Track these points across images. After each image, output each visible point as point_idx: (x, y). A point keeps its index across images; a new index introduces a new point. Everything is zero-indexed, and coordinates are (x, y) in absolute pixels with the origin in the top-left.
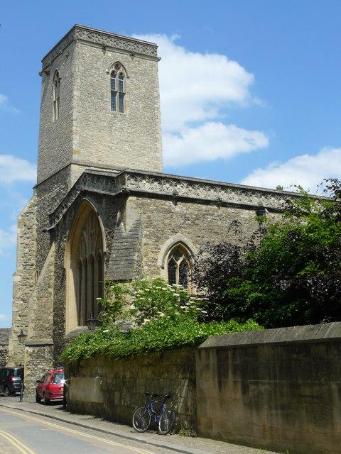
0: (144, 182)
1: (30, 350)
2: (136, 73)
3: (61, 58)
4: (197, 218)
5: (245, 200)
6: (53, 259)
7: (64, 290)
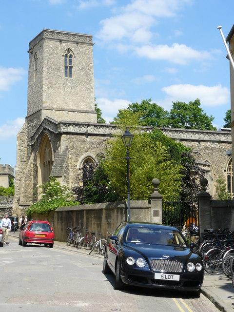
0: (70, 127)
1: (21, 208)
3: (38, 46)
6: (32, 161)
7: (37, 178)
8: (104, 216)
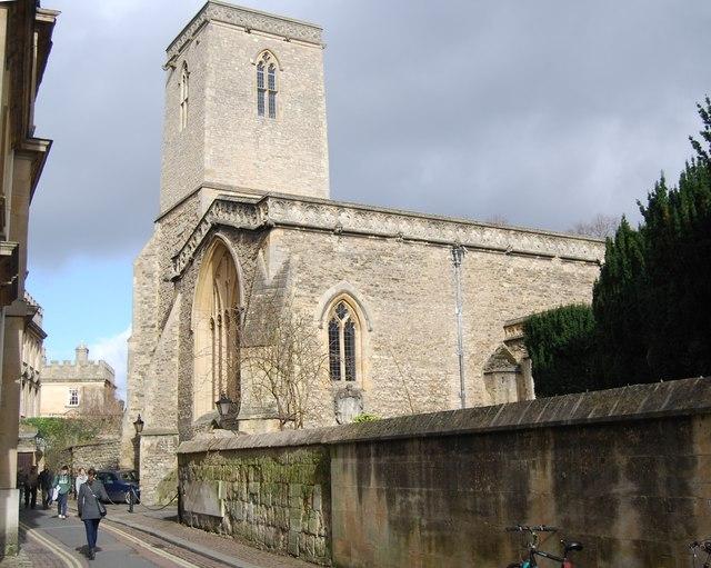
4: (369, 260)
5: (435, 234)
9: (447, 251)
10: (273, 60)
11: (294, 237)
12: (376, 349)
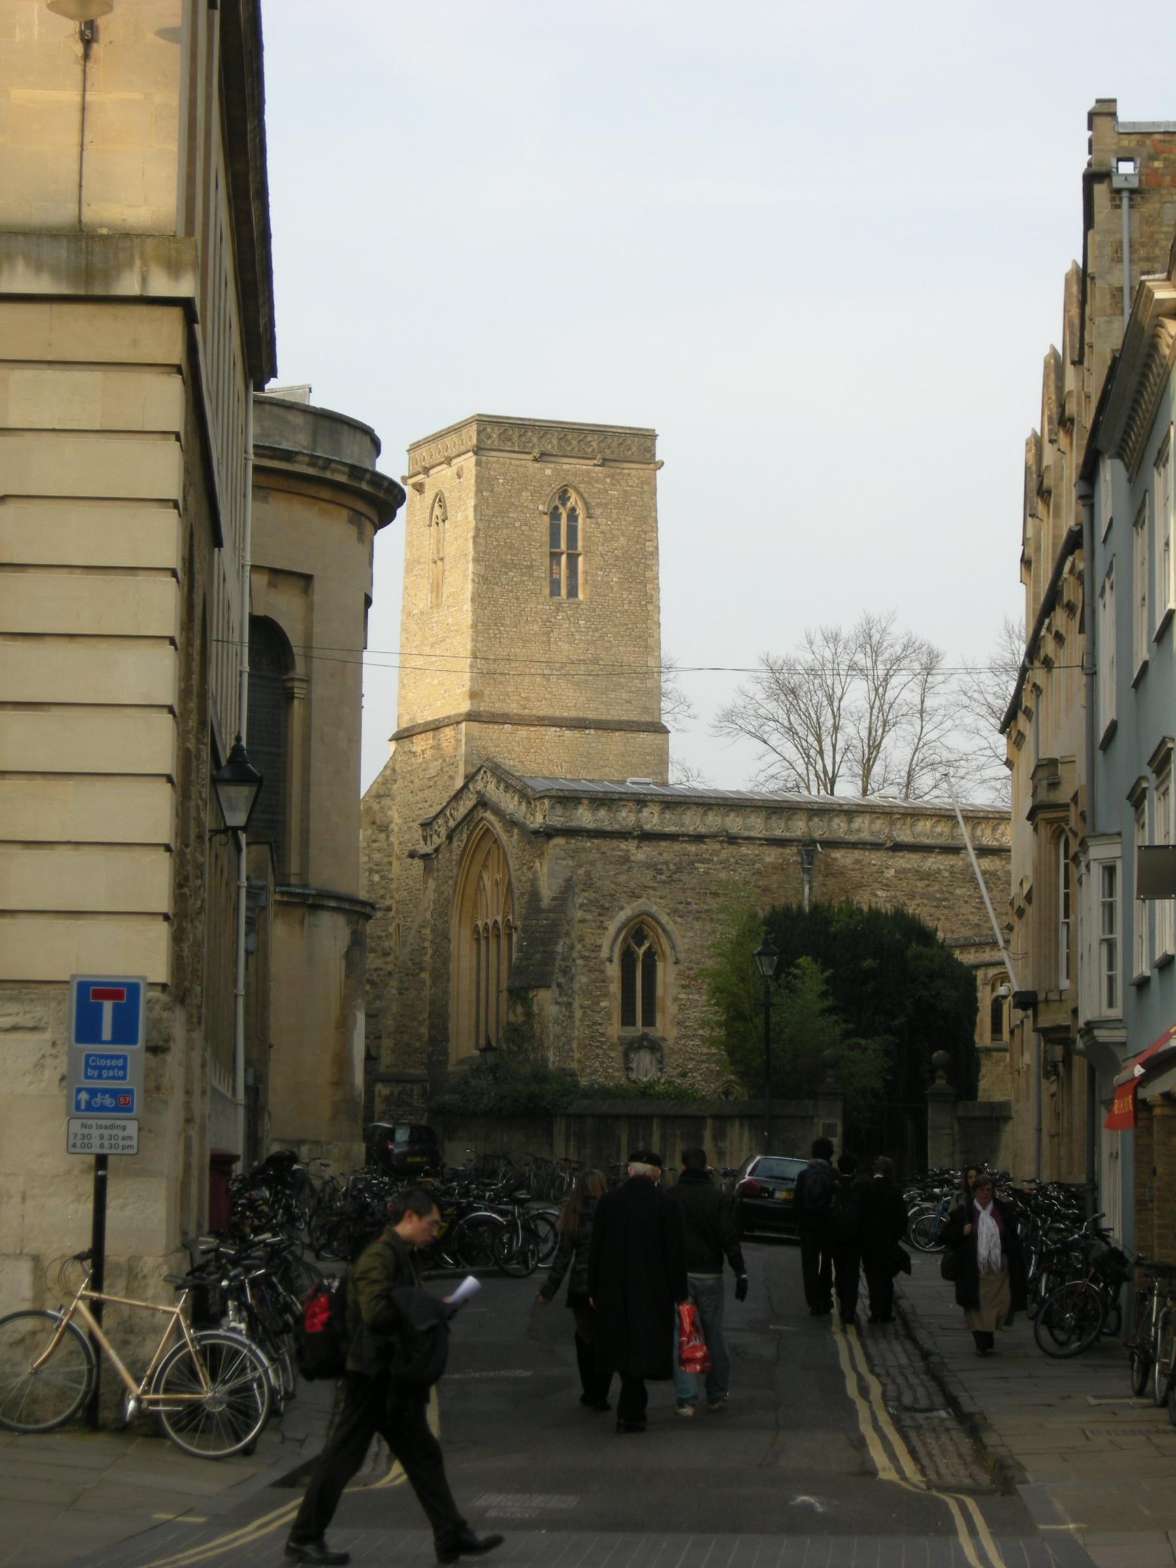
2: (605, 506)
4: (678, 870)
6: (428, 916)
8: (707, 1134)
9: (791, 853)
10: (573, 499)
11: (579, 844)
12: (684, 987)
